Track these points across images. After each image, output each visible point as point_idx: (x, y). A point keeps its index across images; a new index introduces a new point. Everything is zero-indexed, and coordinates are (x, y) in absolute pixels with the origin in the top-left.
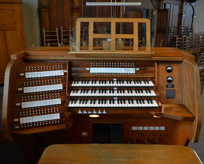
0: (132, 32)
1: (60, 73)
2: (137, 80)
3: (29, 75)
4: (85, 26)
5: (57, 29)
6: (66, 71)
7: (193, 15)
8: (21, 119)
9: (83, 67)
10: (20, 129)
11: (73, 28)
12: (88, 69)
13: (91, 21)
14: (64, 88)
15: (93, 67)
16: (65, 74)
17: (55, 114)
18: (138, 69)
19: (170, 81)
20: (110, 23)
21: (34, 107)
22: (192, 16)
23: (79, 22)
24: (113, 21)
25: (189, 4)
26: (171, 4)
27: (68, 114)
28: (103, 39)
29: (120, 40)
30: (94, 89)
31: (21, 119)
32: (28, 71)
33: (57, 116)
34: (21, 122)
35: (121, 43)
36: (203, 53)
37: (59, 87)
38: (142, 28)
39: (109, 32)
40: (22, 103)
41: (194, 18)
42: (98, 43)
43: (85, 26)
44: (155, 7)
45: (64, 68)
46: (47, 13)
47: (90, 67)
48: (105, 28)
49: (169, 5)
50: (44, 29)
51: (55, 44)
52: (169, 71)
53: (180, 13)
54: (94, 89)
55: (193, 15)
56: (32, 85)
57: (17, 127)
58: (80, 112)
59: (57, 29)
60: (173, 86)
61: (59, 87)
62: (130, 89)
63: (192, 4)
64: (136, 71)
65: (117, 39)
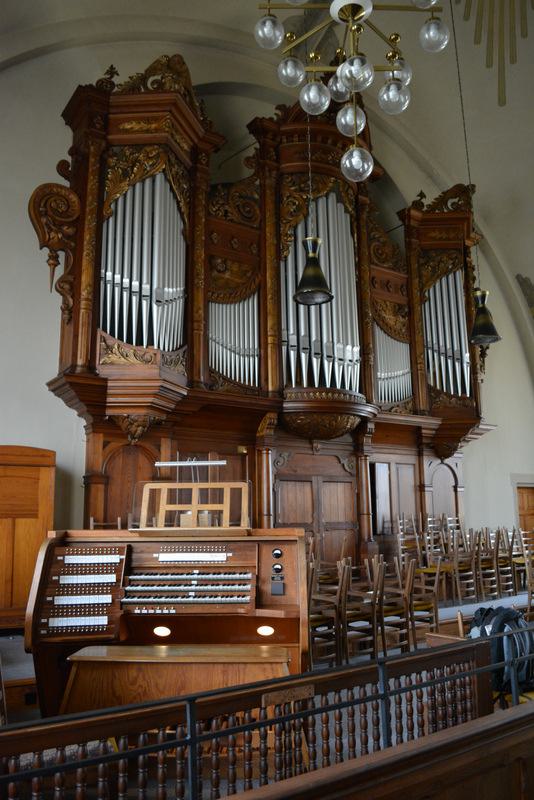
0: (221, 502)
1: (115, 559)
2: (230, 570)
3: (71, 559)
4: (154, 494)
5: (119, 519)
6: (124, 557)
7: (455, 488)
8: (51, 619)
9: (149, 552)
10: (49, 635)
11: (154, 519)
12: (155, 555)
13: (164, 487)
14: (118, 580)
15: (163, 552)
16: (121, 560)
17: (101, 617)
18: (230, 555)
19: (278, 571)
20: (191, 490)
21: (72, 605)
22: (452, 489)
23: (148, 487)
24: (195, 487)
25: (439, 461)
26: (389, 464)
27: (119, 613)
28: (182, 512)
29: (206, 512)
30: (162, 583)
31: (51, 619)
32: (69, 554)
33: (103, 620)
34: (51, 625)
35: (205, 516)
36: (520, 600)
37: (112, 578)
38: (236, 495)
39: (189, 502)
40: (56, 598)
41: (459, 494)
42: (172, 519)
43: (154, 494)
44: (346, 470)
45: (120, 553)
46: (102, 487)
47: (158, 552)
48: (185, 497)
49: (386, 465)
50: (92, 520)
51: (134, 712)
52: (278, 556)
53: (418, 484)
54: (162, 583)
55: (455, 488)
56: (73, 574)
57: (43, 632)
58: (137, 611)
59: (119, 519)
60: (282, 578)
61: (112, 578)
62: (215, 583)
63: (447, 461)
64: (227, 558)
65: (199, 512)
